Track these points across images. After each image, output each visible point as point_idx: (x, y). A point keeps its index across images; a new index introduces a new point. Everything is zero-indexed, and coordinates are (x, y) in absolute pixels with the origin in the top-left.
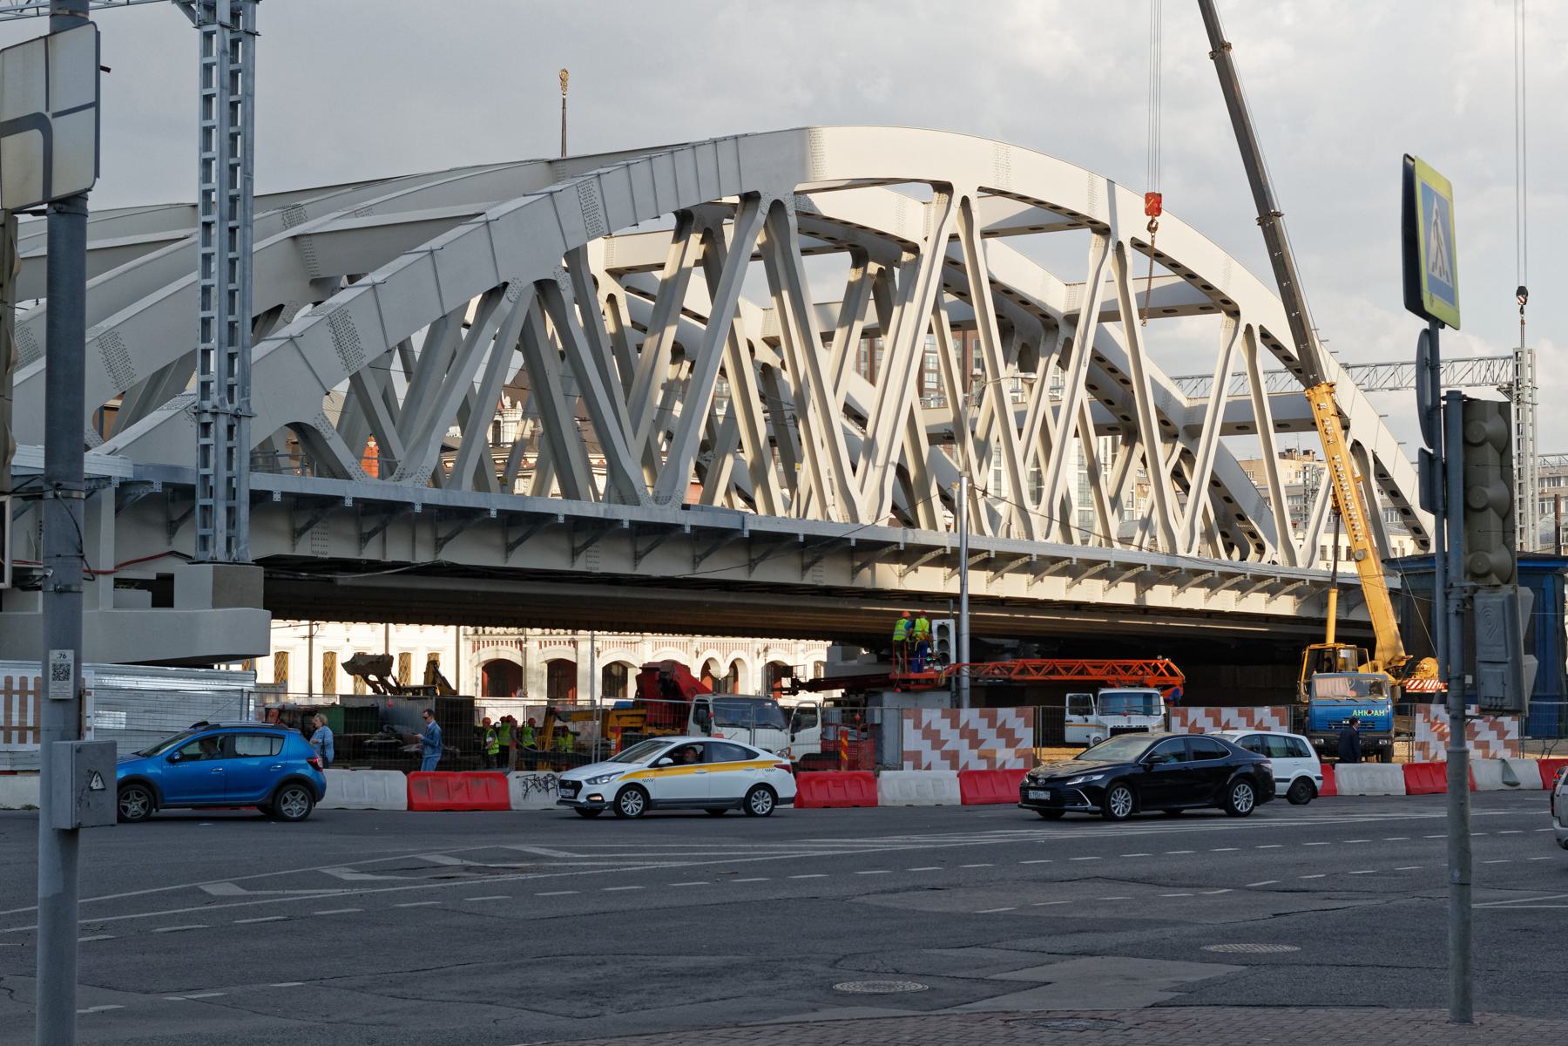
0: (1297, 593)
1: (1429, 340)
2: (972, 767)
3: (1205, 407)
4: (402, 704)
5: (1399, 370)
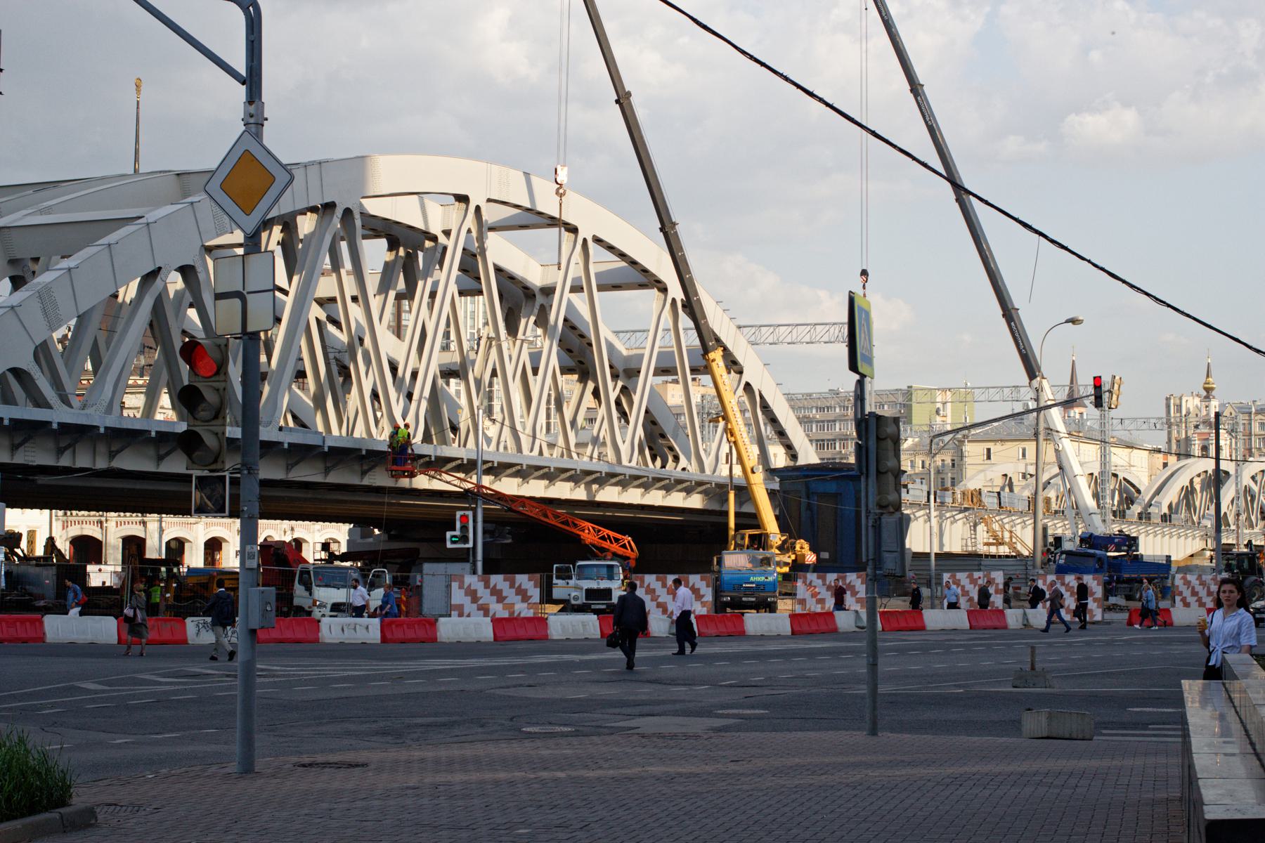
0: (705, 493)
1: (860, 384)
2: (498, 616)
3: (642, 355)
4: (32, 570)
5: (777, 330)
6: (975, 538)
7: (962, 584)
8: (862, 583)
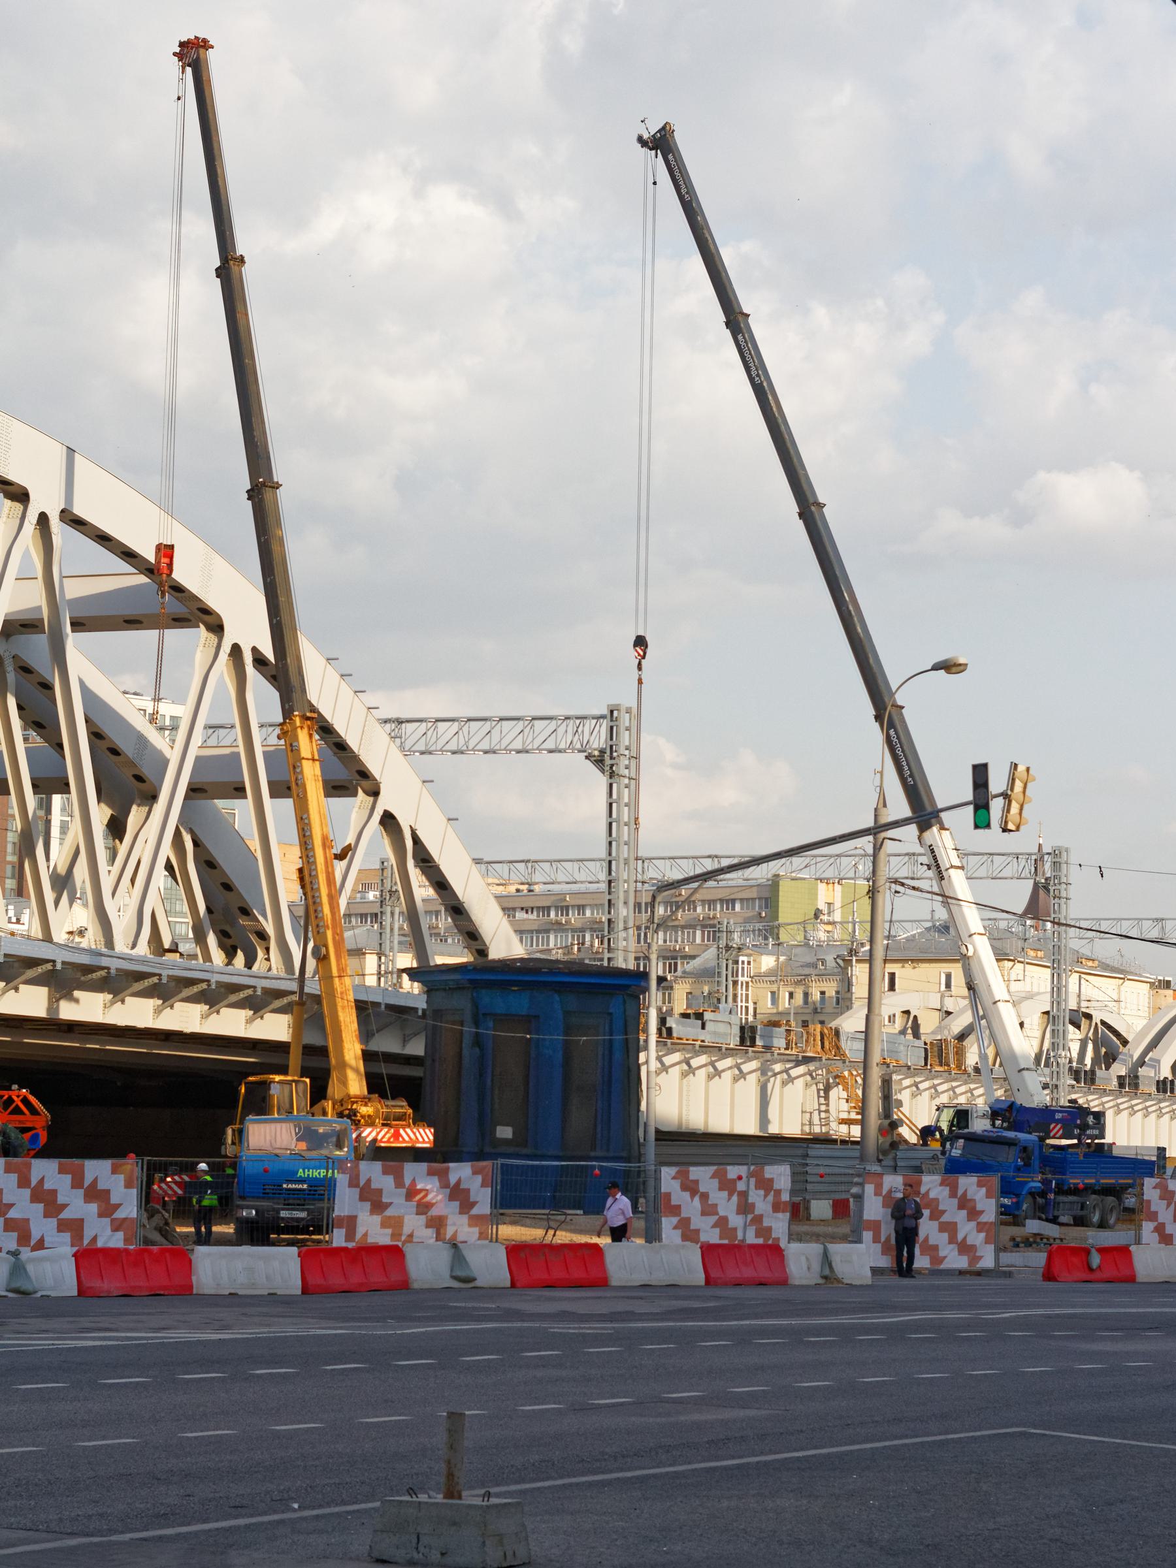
5: (465, 729)
6: (827, 1111)
7: (702, 1189)
8: (483, 1185)
